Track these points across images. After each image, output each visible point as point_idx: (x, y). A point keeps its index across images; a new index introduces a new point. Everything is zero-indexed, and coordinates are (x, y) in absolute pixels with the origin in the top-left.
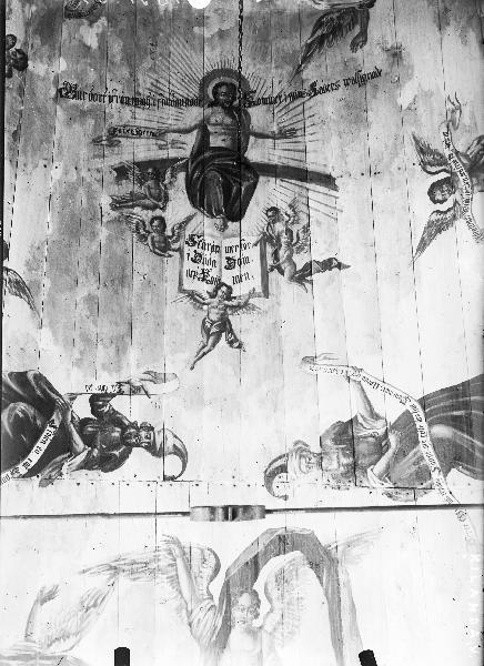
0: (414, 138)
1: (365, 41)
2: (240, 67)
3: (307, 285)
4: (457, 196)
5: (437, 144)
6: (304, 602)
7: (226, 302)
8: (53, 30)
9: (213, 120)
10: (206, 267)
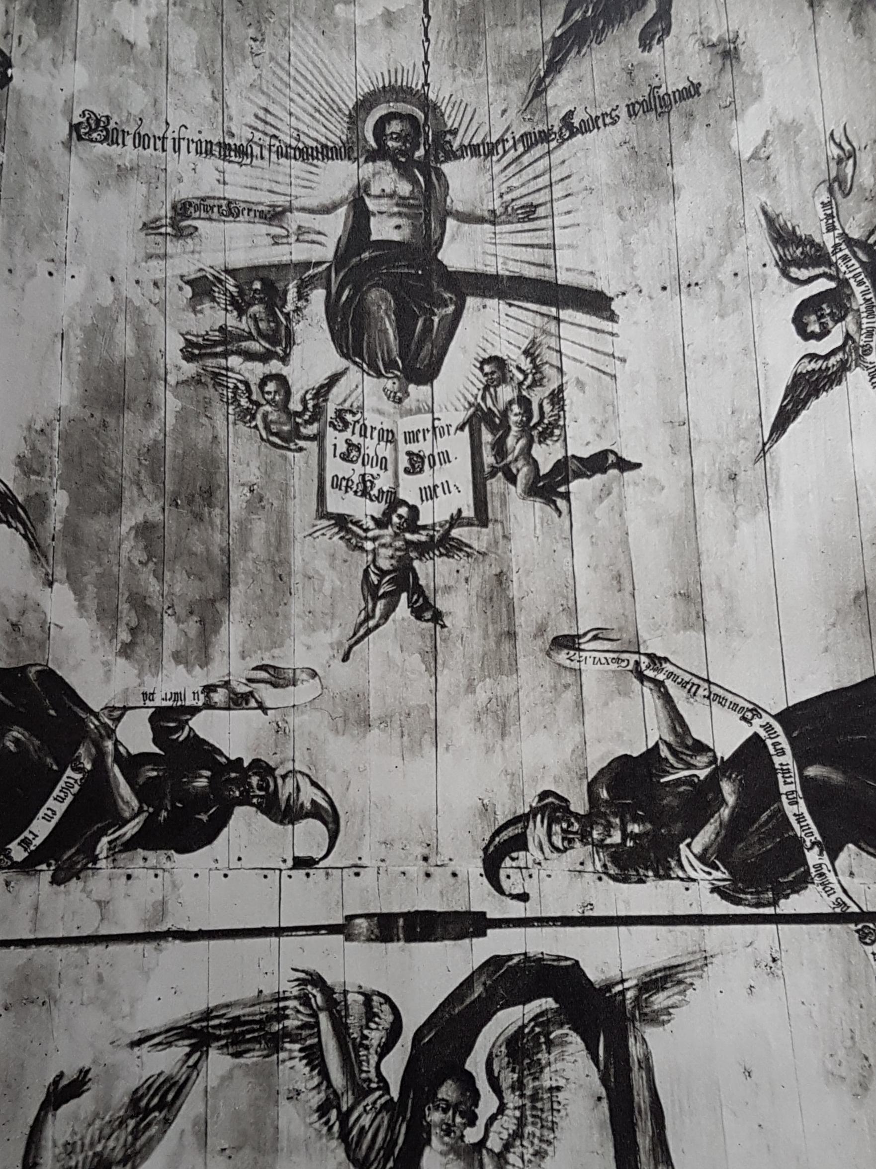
0: (765, 213)
1: (667, 31)
2: (426, 83)
3: (561, 503)
4: (850, 323)
5: (810, 224)
6: (561, 1096)
7: (408, 536)
8: (60, 19)
9: (375, 190)
10: (368, 470)
